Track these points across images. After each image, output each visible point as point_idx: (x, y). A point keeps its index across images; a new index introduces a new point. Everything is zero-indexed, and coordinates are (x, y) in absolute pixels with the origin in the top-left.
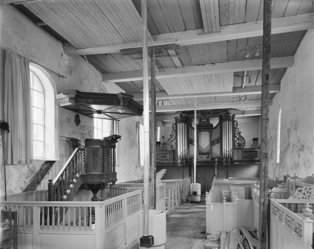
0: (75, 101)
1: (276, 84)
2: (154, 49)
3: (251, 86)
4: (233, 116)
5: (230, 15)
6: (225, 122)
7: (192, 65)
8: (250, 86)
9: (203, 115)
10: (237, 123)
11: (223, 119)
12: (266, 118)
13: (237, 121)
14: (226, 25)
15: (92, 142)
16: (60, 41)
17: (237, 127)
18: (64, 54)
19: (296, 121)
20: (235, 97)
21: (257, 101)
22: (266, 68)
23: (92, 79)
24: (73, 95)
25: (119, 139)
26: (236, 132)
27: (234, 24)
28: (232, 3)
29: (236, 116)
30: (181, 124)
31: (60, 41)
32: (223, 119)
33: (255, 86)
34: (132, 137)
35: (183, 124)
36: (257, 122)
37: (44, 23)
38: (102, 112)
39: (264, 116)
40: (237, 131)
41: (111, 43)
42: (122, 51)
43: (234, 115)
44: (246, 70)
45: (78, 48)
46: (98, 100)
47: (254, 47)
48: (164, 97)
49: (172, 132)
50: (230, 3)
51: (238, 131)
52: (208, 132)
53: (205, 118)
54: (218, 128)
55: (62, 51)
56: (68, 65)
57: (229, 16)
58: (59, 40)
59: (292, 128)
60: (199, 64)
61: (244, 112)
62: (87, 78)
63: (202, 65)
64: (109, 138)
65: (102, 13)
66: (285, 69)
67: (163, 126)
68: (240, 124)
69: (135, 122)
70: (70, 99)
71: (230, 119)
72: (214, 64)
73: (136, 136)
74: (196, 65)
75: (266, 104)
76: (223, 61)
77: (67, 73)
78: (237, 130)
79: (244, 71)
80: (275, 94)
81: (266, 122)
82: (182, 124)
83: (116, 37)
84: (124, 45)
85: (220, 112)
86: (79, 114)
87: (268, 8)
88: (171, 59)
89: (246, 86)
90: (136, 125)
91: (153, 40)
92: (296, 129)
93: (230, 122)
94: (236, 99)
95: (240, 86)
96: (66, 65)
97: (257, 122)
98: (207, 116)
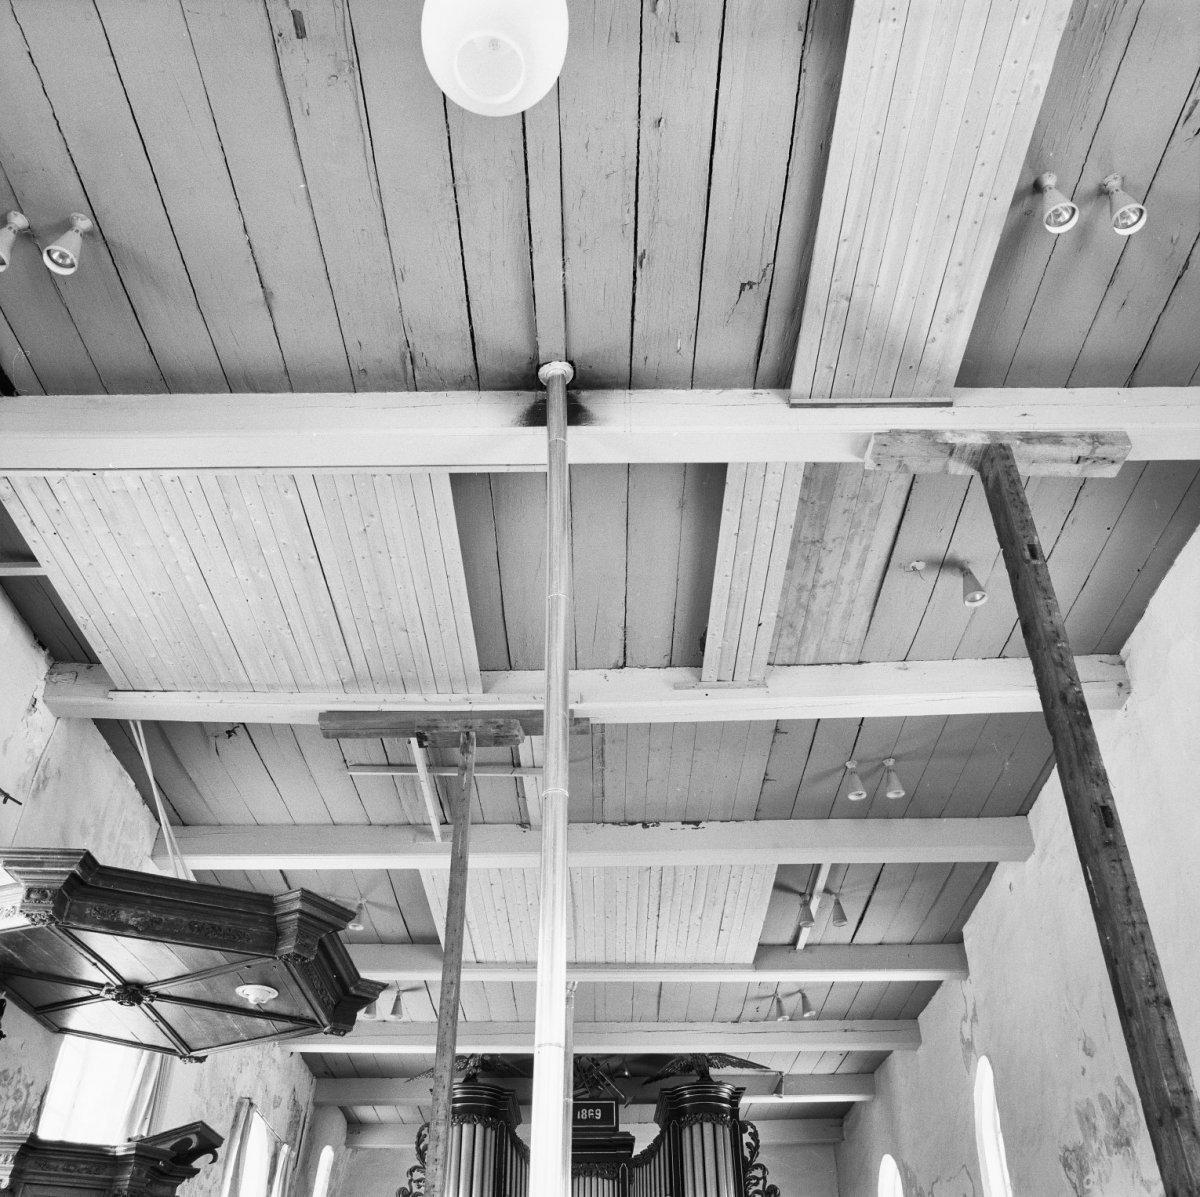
0: (53, 909)
1: (942, 942)
2: (479, 722)
3: (834, 944)
4: (732, 1097)
5: (809, 626)
6: (696, 1128)
7: (600, 819)
8: (830, 945)
9: (584, 1086)
10: (754, 1136)
11: (682, 1112)
12: (1157, 998)
13: (753, 1127)
14: (787, 662)
15: (52, 1164)
16: (44, 653)
17: (758, 1161)
18: (40, 705)
19: (1114, 1105)
20: (754, 992)
21: (848, 1024)
22: (1092, 781)
23: (112, 836)
24: (56, 877)
25: (210, 1157)
26: (754, 1188)
27: (819, 664)
28: (824, 586)
29: (745, 1101)
30: (465, 1126)
31: (47, 651)
32: (682, 1112)
33: (849, 945)
34: (201, 1189)
35: (479, 1128)
36: (829, 1144)
37: (30, 558)
38: (147, 993)
39: (1145, 989)
40: (758, 1179)
41: (289, 679)
42: (326, 716)
43: (737, 1093)
44: (826, 858)
45: (119, 688)
46: (172, 918)
47: (877, 764)
48: (411, 968)
49: (411, 1171)
50: (821, 582)
51: (761, 1182)
52: (608, 1179)
53: (590, 1099)
54: (661, 1161)
55: (39, 695)
56: (38, 753)
57: (804, 627)
58: (44, 649)
59: (1095, 1146)
60: (630, 818)
61: (781, 1081)
62: (93, 830)
63: (645, 825)
64: (164, 1142)
65: (315, 554)
66: (989, 869)
67: (349, 1143)
68: (765, 1146)
69: (232, 1098)
70: (32, 896)
71: (723, 1110)
72: (697, 823)
73: (222, 1183)
74: (613, 823)
75: (1137, 930)
76: (736, 817)
77: (24, 786)
78: (758, 1173)
79: (818, 867)
80: (937, 984)
81: (1163, 1018)
82: (471, 1126)
83: (324, 659)
84: (343, 697)
85: (668, 1075)
86: (7, 1000)
87: (1038, 579)
88: (518, 782)
89: (811, 941)
90: (232, 1116)
91: (481, 690)
92: (1128, 1143)
93: (719, 1129)
94: (757, 1004)
95: (787, 938)
96: (30, 751)
97: (829, 1144)
98: (608, 1092)
